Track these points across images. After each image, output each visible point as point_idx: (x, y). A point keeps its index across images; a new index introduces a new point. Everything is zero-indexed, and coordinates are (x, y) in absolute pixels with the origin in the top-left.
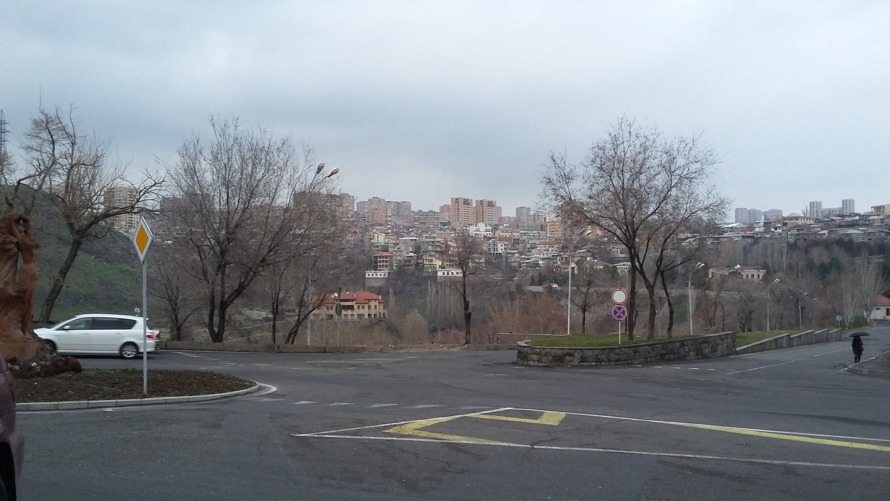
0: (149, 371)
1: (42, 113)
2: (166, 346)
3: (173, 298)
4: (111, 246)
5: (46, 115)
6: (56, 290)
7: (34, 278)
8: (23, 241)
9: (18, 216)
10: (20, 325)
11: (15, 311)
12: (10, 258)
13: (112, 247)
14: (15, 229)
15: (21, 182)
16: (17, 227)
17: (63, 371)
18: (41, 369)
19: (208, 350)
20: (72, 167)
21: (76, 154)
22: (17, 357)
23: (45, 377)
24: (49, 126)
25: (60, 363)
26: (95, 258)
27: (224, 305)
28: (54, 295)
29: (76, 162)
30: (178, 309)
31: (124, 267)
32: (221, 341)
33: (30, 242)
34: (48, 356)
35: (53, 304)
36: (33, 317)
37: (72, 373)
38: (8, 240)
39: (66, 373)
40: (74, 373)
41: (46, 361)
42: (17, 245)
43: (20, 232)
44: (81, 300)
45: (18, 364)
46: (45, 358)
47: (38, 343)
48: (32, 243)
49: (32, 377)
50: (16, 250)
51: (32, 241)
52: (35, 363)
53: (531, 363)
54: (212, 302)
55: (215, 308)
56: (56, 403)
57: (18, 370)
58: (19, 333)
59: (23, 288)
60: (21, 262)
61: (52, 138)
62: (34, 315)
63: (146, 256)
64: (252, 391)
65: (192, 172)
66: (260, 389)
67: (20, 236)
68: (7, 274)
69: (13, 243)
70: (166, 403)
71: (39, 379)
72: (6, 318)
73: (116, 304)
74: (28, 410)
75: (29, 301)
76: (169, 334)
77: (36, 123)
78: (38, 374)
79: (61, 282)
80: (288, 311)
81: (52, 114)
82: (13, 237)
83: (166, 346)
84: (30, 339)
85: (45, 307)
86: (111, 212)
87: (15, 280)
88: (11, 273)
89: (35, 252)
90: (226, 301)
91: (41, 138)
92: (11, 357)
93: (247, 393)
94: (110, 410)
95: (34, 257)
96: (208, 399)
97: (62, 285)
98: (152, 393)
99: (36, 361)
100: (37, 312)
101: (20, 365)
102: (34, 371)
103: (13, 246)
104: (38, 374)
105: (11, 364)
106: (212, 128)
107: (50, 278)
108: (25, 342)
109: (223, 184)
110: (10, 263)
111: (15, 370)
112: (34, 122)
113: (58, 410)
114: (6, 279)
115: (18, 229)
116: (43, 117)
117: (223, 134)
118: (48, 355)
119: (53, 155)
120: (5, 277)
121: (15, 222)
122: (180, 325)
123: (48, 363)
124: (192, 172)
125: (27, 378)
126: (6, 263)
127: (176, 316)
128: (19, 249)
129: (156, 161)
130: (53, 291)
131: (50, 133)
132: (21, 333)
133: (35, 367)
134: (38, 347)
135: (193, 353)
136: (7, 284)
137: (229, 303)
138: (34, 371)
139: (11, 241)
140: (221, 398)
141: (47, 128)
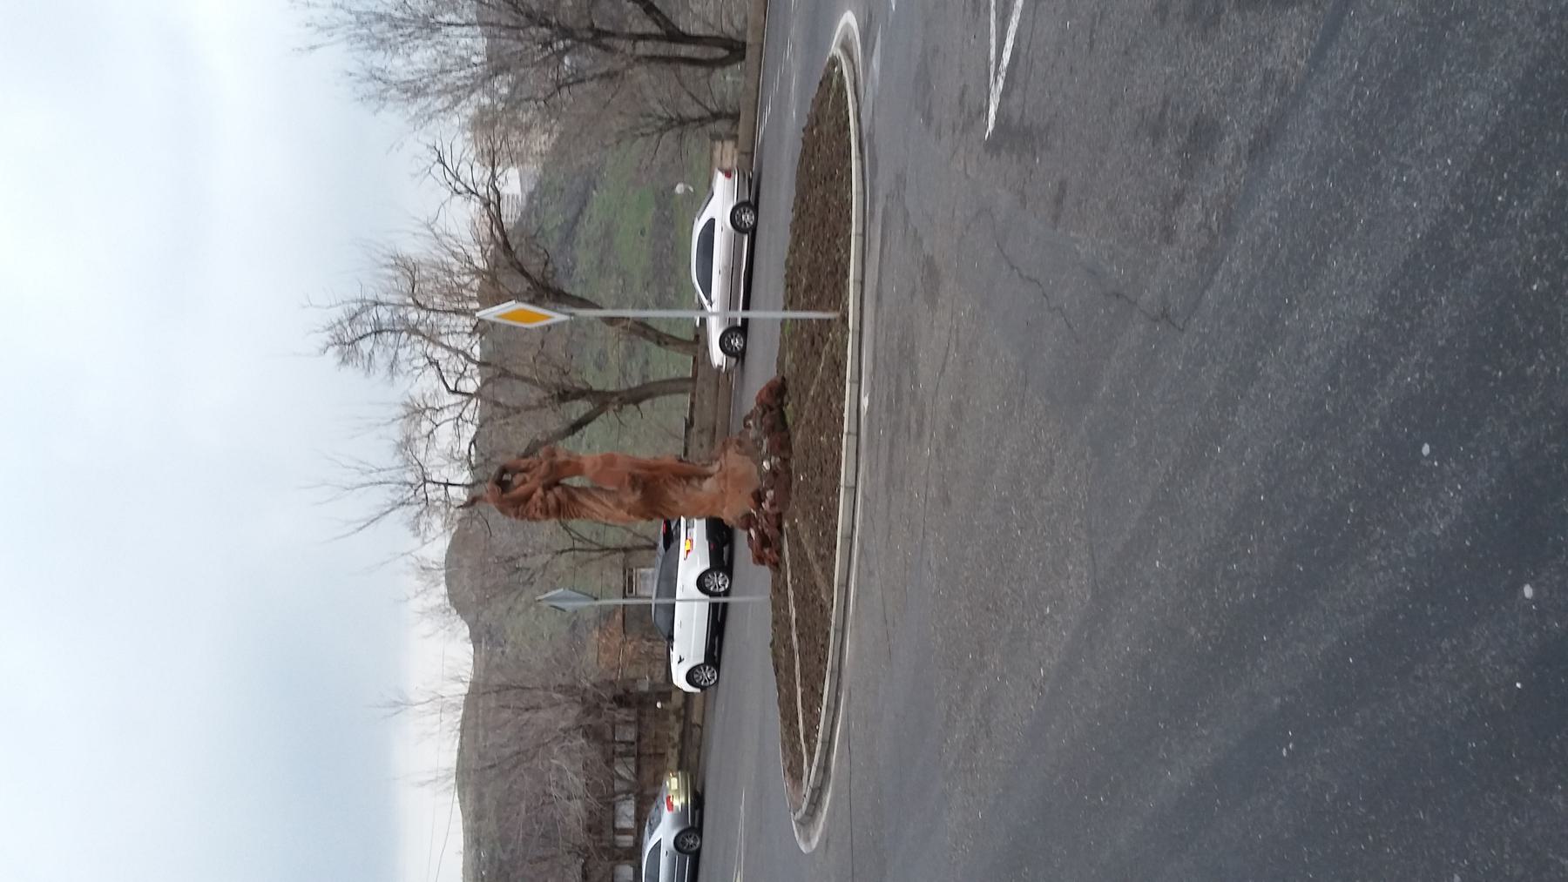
0: (790, 304)
2: (746, 154)
5: (328, 345)
7: (609, 461)
8: (542, 478)
9: (496, 488)
10: (695, 482)
12: (572, 499)
14: (522, 490)
15: (452, 387)
16: (516, 488)
17: (782, 415)
18: (776, 456)
19: (759, 76)
21: (394, 298)
27: (675, 36)
28: (649, 333)
38: (539, 504)
39: (786, 412)
42: (548, 488)
43: (524, 482)
45: (765, 490)
47: (729, 452)
48: (545, 464)
49: (789, 471)
50: (557, 490)
52: (764, 464)
53: (908, 572)
58: (708, 484)
60: (576, 481)
61: (371, 334)
64: (856, 109)
65: (414, 90)
66: (846, 47)
68: (603, 504)
69: (546, 494)
70: (862, 283)
72: (681, 504)
74: (851, 537)
75: (649, 468)
76: (726, 143)
78: (785, 461)
81: (326, 337)
82: (534, 497)
83: (746, 154)
84: (721, 466)
86: (500, 239)
87: (613, 492)
88: (599, 497)
92: (752, 501)
93: (856, 93)
94: (865, 402)
95: (572, 459)
96: (860, 189)
98: (836, 298)
102: (778, 467)
103: (550, 496)
104: (785, 461)
106: (318, 51)
108: (725, 477)
110: (582, 498)
113: (855, 488)
114: (610, 505)
116: (333, 351)
117: (329, 29)
120: (609, 508)
122: (709, 114)
124: (414, 90)
125: (791, 481)
126: (583, 505)
128: (557, 484)
129: (398, 150)
130: (644, 335)
134: (737, 452)
135: (763, 110)
136: (620, 505)
137: (671, 28)
138: (778, 467)
139: (542, 500)
140: (862, 158)
141: (353, 342)
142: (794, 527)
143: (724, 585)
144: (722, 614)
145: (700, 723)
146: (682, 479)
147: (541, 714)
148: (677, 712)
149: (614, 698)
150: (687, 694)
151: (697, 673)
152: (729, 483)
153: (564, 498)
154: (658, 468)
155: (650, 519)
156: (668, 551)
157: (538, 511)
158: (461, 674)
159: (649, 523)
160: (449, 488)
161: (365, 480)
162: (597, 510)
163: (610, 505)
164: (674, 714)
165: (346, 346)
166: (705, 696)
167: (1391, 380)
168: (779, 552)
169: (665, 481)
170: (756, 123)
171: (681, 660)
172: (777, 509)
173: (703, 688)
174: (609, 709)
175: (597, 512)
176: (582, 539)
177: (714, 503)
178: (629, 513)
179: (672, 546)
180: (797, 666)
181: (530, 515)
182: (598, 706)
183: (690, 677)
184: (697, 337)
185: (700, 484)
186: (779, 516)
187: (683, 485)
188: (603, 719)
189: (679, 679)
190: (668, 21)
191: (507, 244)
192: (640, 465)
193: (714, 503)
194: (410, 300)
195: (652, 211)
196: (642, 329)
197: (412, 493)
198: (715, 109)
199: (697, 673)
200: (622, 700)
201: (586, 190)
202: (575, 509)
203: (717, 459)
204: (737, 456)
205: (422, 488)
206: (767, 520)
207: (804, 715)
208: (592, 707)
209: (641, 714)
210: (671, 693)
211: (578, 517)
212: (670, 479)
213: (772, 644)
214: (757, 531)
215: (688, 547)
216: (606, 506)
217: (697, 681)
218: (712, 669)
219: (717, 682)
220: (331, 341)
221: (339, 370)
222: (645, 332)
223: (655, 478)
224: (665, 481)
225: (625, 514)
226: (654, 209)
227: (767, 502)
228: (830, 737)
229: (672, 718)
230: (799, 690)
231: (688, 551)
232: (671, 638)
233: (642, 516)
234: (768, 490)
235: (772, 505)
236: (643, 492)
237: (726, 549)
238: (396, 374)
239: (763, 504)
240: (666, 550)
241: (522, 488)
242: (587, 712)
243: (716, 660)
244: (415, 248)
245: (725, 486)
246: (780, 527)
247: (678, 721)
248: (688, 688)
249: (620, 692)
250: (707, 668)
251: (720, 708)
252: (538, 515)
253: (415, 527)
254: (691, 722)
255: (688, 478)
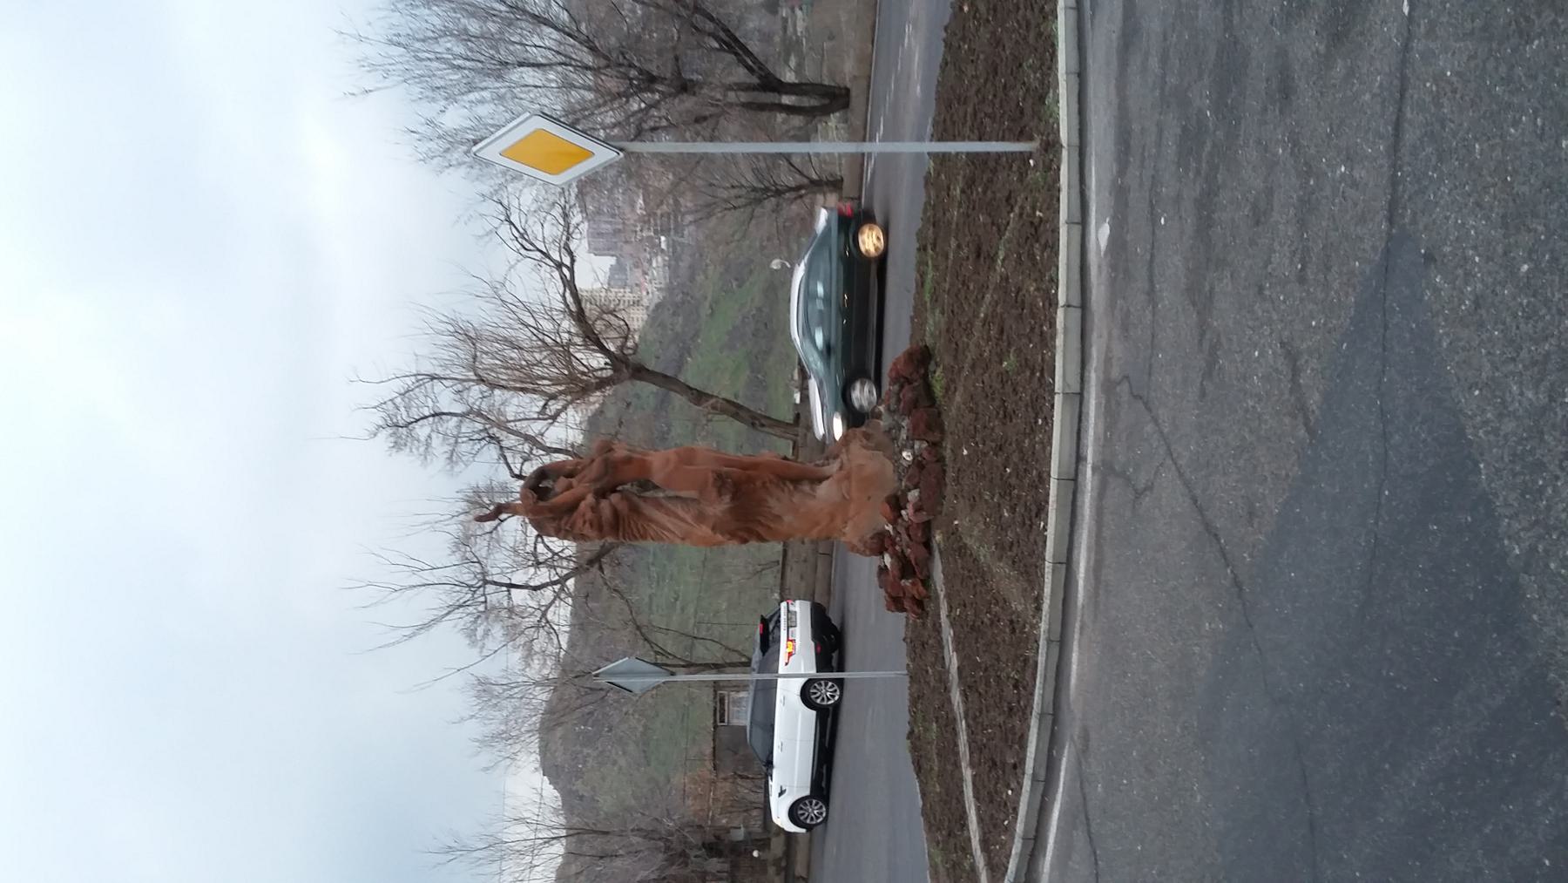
1: (375, 435)
3: (752, 195)
4: (670, 332)
6: (734, 409)
9: (530, 494)
10: (806, 487)
11: (769, 499)
12: (635, 509)
13: (672, 330)
17: (928, 388)
20: (481, 380)
21: (459, 372)
22: (885, 495)
23: (942, 431)
24: (401, 423)
25: (908, 394)
26: (690, 356)
28: (742, 413)
29: (472, 373)
30: (776, 184)
31: (705, 310)
32: (848, 90)
33: (595, 464)
34: (884, 423)
35: (760, 415)
36: (785, 458)
37: (932, 367)
38: (589, 515)
40: (933, 363)
41: (900, 428)
42: (601, 494)
43: (570, 487)
44: (759, 376)
45: (905, 493)
46: (890, 429)
48: (598, 460)
49: (941, 460)
50: (614, 498)
51: (593, 461)
54: (762, 107)
55: (777, 102)
56: (1058, 400)
57: (920, 492)
58: (823, 489)
59: (711, 480)
62: (782, 454)
63: (606, 142)
67: (580, 486)
69: (598, 503)
71: (948, 445)
72: (788, 518)
73: (766, 324)
77: (397, 446)
78: (935, 445)
79: (717, 402)
80: (785, 29)
81: (377, 418)
82: (583, 504)
85: (766, 429)
86: (573, 308)
87: (693, 500)
88: (673, 508)
89: (620, 452)
90: (760, 77)
91: (429, 437)
97: (724, 399)
99: (897, 450)
100: (776, 448)
101: (906, 486)
102: (925, 455)
103: (604, 504)
104: (935, 445)
105: (905, 508)
107: (709, 421)
108: (848, 477)
109: (499, 77)
111: (920, 499)
112: (394, 450)
114: (688, 518)
115: (561, 493)
116: (384, 434)
118: (882, 423)
119: (463, 415)
120: (687, 522)
121: (542, 500)
123: (904, 424)
126: (651, 520)
127: (791, 189)
129: (466, 224)
130: (736, 416)
131: (417, 421)
132: (825, 484)
133: (913, 454)
134: (865, 447)
136: (701, 518)
141: (407, 425)
142: (953, 534)
143: (833, 696)
144: (830, 738)
145: (804, 875)
146: (788, 483)
147: (618, 863)
148: (776, 862)
149: (703, 844)
150: (789, 835)
151: (802, 809)
152: (854, 484)
153: (623, 507)
154: (755, 466)
155: (745, 541)
156: (767, 654)
157: (587, 525)
158: (526, 815)
159: (744, 547)
160: (513, 591)
161: (415, 580)
162: (669, 526)
163: (688, 518)
164: (774, 865)
165: (400, 429)
166: (811, 841)
167: (1077, 867)
168: (926, 582)
169: (764, 483)
170: (863, 164)
171: (781, 793)
172: (924, 517)
173: (809, 828)
174: (696, 857)
175: (669, 530)
176: (664, 653)
177: (832, 517)
178: (713, 529)
179: (770, 651)
180: (963, 738)
181: (576, 531)
182: (683, 854)
183: (793, 813)
184: (798, 416)
185: (813, 490)
186: (927, 527)
187: (790, 491)
188: (690, 867)
189: (780, 817)
190: (761, 67)
191: (581, 311)
192: (730, 463)
193: (832, 517)
194: (471, 375)
195: (745, 375)
196: (733, 409)
197: (469, 596)
198: (814, 177)
199: (802, 809)
200: (714, 847)
201: (681, 356)
202: (639, 526)
203: (836, 457)
204: (864, 451)
205: (482, 589)
206: (909, 536)
207: (978, 809)
208: (678, 856)
209: (735, 866)
210: (769, 839)
211: (644, 537)
212: (771, 481)
213: (911, 734)
214: (894, 555)
215: (789, 650)
216: (683, 520)
217: (802, 818)
218: (820, 804)
219: (826, 819)
220: (381, 423)
221: (390, 455)
222: (737, 414)
223: (750, 480)
224: (764, 483)
225: (710, 532)
226: (748, 372)
227: (910, 507)
228: (1037, 831)
229: (771, 870)
230: (968, 774)
231: (790, 654)
232: (769, 764)
233: (733, 535)
234: (910, 490)
235: (918, 509)
236: (733, 499)
237: (835, 655)
238: (457, 463)
239: (903, 512)
240: (764, 655)
241: (566, 493)
242: (671, 861)
243: (825, 792)
244: (482, 314)
245: (849, 492)
246: (927, 545)
247: (778, 874)
248: (790, 827)
249: (710, 838)
250: (814, 801)
251: (831, 848)
252: (587, 530)
253: (471, 634)
254: (794, 875)
255: (797, 481)
